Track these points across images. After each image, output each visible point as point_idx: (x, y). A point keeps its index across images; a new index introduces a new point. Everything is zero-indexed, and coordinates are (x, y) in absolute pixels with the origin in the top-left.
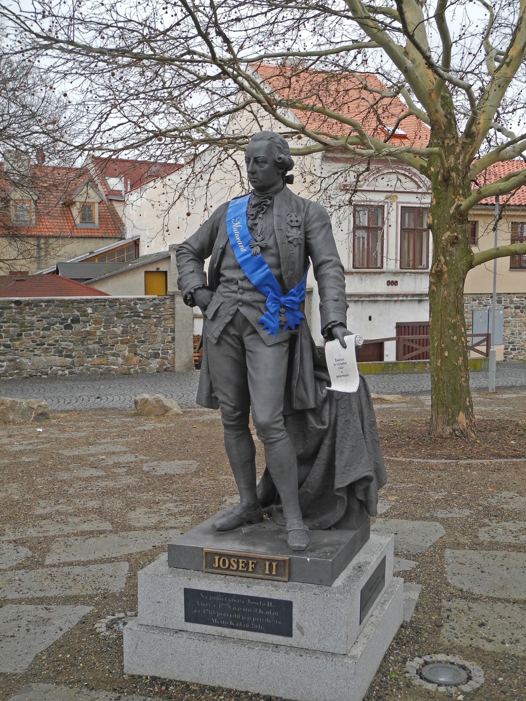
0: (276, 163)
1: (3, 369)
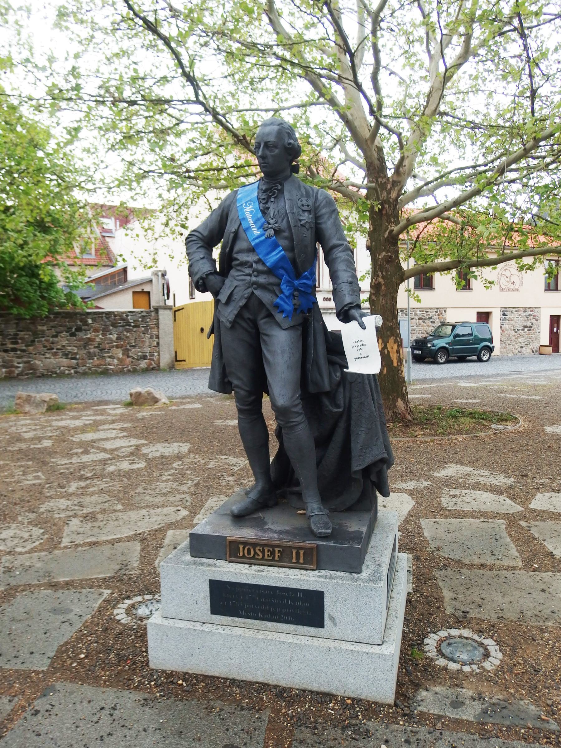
1: (20, 369)
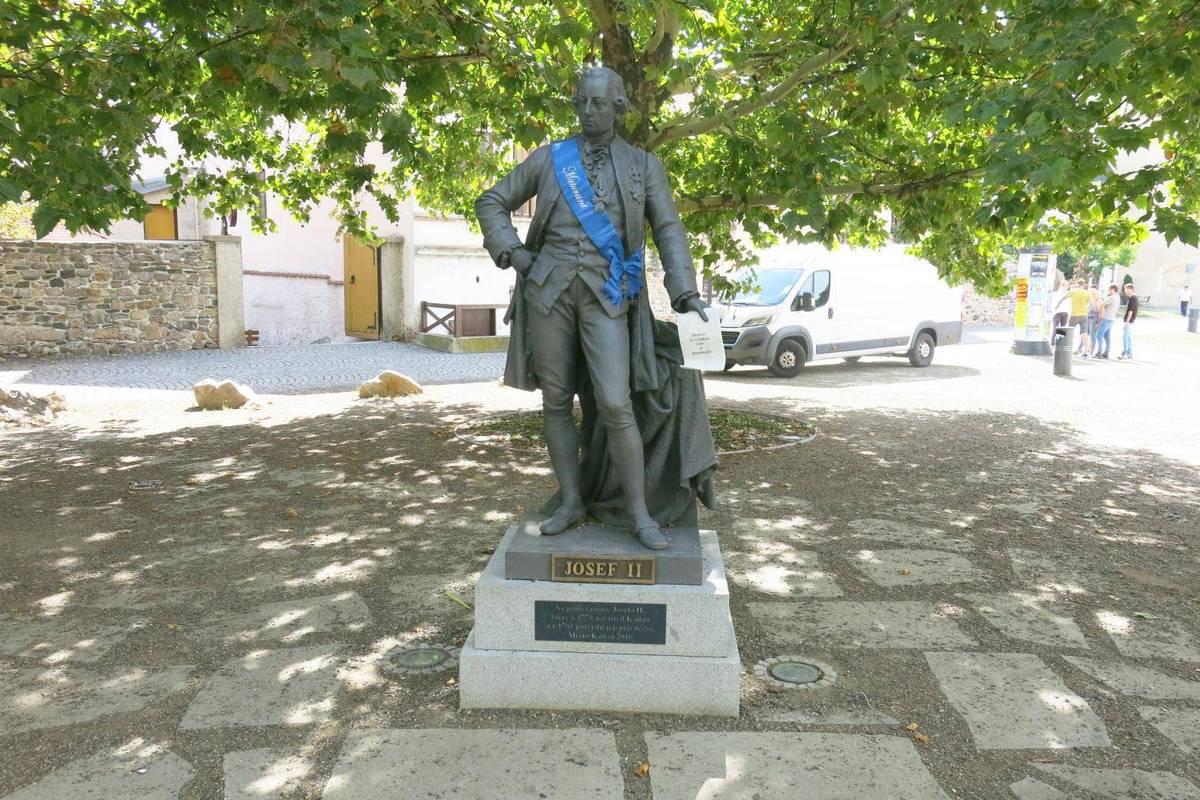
0: (615, 105)
